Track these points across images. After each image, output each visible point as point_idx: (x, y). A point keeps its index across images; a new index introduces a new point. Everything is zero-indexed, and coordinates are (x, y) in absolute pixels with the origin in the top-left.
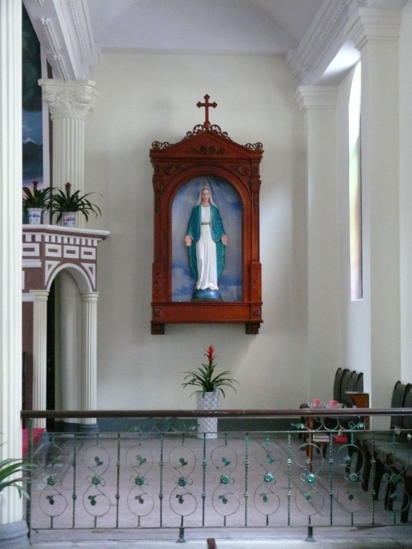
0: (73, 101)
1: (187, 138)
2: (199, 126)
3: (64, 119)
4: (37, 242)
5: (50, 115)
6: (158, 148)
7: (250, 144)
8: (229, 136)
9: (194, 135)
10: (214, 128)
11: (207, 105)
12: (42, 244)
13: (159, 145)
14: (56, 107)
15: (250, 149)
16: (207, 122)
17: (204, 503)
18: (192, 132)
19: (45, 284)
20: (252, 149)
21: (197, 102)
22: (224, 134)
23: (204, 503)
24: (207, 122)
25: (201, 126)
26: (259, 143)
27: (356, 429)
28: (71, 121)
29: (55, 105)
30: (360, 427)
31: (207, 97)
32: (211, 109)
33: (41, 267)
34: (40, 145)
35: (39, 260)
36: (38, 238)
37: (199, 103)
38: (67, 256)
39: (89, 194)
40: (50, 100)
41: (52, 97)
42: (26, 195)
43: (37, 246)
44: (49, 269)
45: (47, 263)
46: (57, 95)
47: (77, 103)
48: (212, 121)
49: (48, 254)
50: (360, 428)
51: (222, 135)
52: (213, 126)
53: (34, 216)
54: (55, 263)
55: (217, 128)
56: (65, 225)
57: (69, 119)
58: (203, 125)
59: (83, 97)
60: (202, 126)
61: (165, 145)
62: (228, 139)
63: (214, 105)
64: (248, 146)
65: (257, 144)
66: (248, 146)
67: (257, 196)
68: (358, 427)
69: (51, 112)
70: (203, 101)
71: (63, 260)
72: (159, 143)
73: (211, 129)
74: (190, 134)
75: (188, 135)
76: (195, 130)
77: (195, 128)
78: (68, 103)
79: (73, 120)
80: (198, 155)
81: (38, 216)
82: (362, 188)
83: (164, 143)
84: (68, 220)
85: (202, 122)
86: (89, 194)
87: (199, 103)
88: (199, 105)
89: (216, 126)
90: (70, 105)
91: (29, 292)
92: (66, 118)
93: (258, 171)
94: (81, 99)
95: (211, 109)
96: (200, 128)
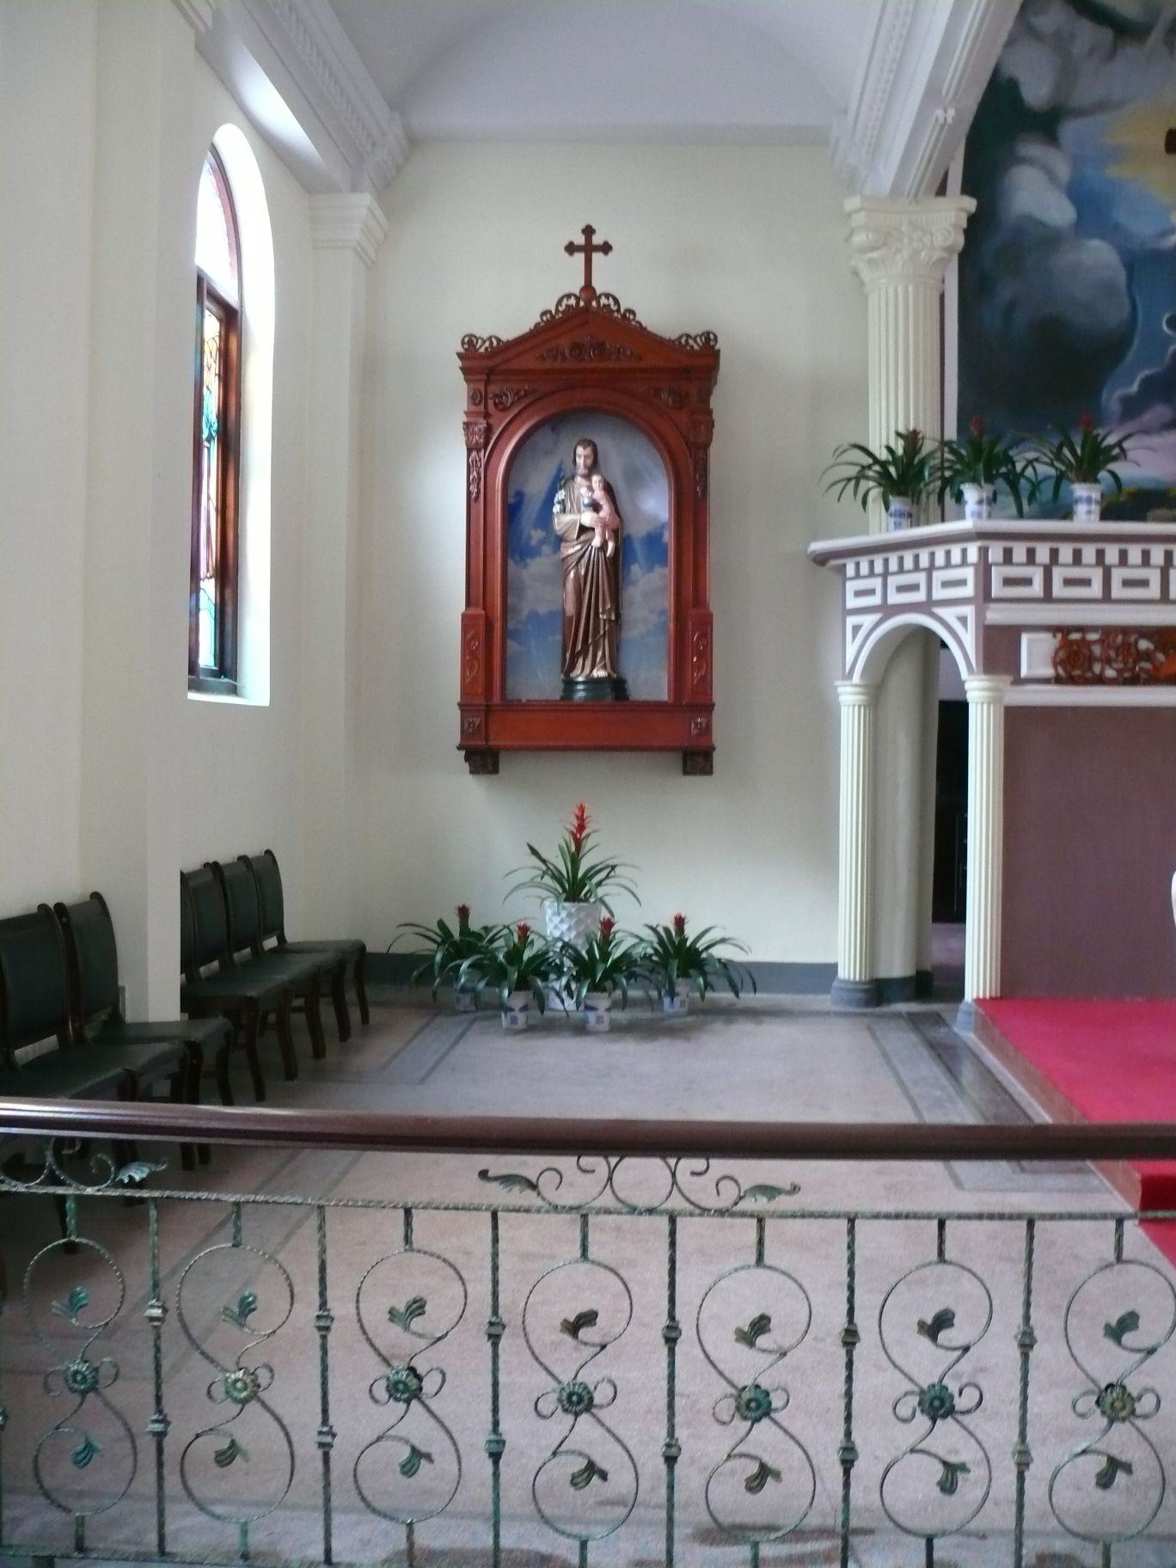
1: (542, 324)
2: (568, 296)
4: (1155, 567)
6: (477, 350)
7: (688, 336)
8: (638, 318)
9: (557, 317)
10: (603, 301)
11: (588, 249)
13: (477, 342)
15: (688, 348)
16: (588, 287)
17: (495, 1356)
18: (553, 312)
20: (692, 347)
21: (566, 243)
22: (627, 315)
23: (495, 1356)
24: (588, 287)
25: (573, 298)
26: (708, 333)
27: (122, 1185)
30: (131, 1178)
31: (589, 231)
32: (597, 257)
37: (571, 244)
38: (895, 598)
44: (854, 637)
48: (599, 286)
50: (133, 1184)
51: (624, 316)
52: (603, 298)
54: (868, 620)
55: (611, 301)
58: (577, 293)
60: (575, 296)
61: (491, 343)
62: (638, 325)
63: (606, 248)
64: (683, 341)
65: (703, 334)
66: (683, 341)
67: (704, 456)
68: (126, 1181)
70: (580, 240)
71: (887, 610)
72: (477, 339)
73: (598, 302)
74: (548, 316)
75: (545, 318)
76: (561, 306)
77: (559, 302)
80: (569, 365)
83: (490, 338)
85: (576, 285)
87: (571, 244)
88: (571, 249)
89: (607, 296)
93: (471, 393)
95: (597, 257)
96: (573, 301)
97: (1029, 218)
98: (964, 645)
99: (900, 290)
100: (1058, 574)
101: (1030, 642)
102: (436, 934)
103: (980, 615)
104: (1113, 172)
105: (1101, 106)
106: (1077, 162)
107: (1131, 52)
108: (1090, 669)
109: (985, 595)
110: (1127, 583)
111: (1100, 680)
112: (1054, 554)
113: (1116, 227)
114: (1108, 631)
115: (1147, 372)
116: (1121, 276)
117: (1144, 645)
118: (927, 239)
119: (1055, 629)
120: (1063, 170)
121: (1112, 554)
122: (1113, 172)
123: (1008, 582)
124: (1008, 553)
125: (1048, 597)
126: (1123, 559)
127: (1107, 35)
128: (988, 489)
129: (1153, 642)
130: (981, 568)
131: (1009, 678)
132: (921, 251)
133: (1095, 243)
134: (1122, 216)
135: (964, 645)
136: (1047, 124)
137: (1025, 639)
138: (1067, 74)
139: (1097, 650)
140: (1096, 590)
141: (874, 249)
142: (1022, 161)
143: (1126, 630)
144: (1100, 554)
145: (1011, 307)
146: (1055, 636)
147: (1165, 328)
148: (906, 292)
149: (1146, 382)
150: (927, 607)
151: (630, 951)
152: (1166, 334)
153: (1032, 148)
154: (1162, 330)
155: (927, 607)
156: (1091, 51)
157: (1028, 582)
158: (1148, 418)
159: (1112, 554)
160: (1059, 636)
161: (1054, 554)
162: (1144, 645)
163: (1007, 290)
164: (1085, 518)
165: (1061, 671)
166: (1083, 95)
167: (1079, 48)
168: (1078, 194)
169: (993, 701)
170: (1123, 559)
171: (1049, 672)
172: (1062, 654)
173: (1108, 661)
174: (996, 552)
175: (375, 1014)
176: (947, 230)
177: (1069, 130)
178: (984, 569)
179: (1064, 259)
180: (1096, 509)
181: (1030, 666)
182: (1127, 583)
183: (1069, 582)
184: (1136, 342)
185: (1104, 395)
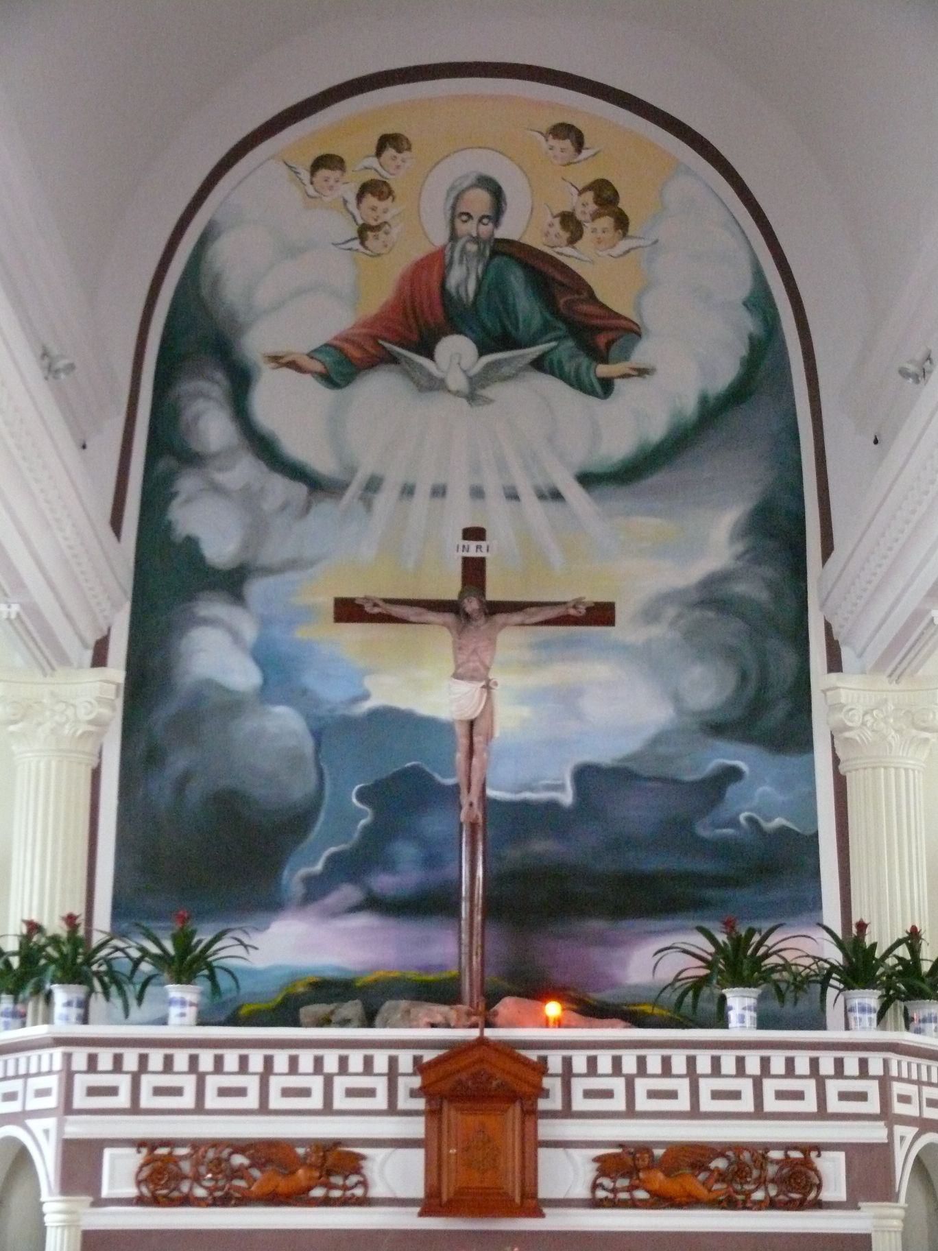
0: (904, 727)
3: (882, 770)
4: (874, 1078)
5: (836, 761)
12: (885, 1082)
14: (862, 740)
19: (897, 1190)
28: (897, 776)
29: (859, 736)
33: (886, 1141)
34: (813, 832)
35: (882, 1123)
36: (876, 1067)
39: (696, 968)
40: (849, 724)
41: (856, 718)
42: (847, 963)
43: (872, 1087)
45: (899, 1130)
46: (865, 713)
47: (914, 732)
49: (899, 1108)
53: (863, 1010)
54: (910, 1131)
56: (918, 1031)
57: (893, 771)
59: (931, 716)
69: (839, 754)
78: (893, 733)
79: (903, 772)
81: (870, 1010)
82: (793, 951)
84: (924, 1021)
86: (696, 968)
90: (898, 737)
91: (859, 1209)
92: (885, 768)
94: (924, 721)
97: (209, 683)
98: (47, 1163)
99: (42, 765)
100: (147, 1082)
101: (113, 1158)
103: (61, 1126)
104: (302, 633)
105: (292, 565)
106: (265, 622)
107: (325, 508)
108: (177, 1188)
109: (68, 1108)
110: (223, 1092)
111: (187, 1201)
112: (143, 1059)
113: (305, 692)
115: (333, 849)
116: (309, 745)
117: (239, 1160)
118: (70, 712)
119: (140, 1144)
120: (249, 632)
121: (206, 1060)
122: (302, 633)
123: (93, 1091)
124: (92, 1060)
125: (135, 1109)
126: (839, 1072)
127: (299, 490)
128: (78, 991)
129: (248, 1157)
130: (64, 1074)
131: (90, 1199)
132: (65, 724)
133: (281, 710)
134: (310, 680)
137: (108, 1153)
138: (257, 530)
139: (186, 1167)
140: (188, 1101)
141: (14, 722)
142: (206, 622)
143: (216, 1144)
144: (194, 1060)
145: (183, 781)
146: (139, 1152)
147: (354, 800)
148: (48, 768)
149: (333, 859)
152: (356, 807)
153: (214, 607)
154: (350, 802)
156: (284, 507)
157: (112, 1091)
159: (331, 1061)
160: (144, 1151)
161: (143, 1059)
162: (239, 1160)
163: (179, 761)
164: (181, 1023)
165: (145, 1190)
166: (274, 551)
167: (270, 504)
168: (264, 656)
169: (68, 1225)
170: (839, 1072)
171: (131, 1191)
172: (146, 1172)
173: (197, 1179)
174: (80, 1058)
176: (90, 703)
177: (256, 589)
178: (69, 1076)
179: (247, 725)
180: (191, 1012)
181: (112, 1186)
182: (223, 1092)
183: (159, 1091)
184: (322, 816)
185: (286, 873)
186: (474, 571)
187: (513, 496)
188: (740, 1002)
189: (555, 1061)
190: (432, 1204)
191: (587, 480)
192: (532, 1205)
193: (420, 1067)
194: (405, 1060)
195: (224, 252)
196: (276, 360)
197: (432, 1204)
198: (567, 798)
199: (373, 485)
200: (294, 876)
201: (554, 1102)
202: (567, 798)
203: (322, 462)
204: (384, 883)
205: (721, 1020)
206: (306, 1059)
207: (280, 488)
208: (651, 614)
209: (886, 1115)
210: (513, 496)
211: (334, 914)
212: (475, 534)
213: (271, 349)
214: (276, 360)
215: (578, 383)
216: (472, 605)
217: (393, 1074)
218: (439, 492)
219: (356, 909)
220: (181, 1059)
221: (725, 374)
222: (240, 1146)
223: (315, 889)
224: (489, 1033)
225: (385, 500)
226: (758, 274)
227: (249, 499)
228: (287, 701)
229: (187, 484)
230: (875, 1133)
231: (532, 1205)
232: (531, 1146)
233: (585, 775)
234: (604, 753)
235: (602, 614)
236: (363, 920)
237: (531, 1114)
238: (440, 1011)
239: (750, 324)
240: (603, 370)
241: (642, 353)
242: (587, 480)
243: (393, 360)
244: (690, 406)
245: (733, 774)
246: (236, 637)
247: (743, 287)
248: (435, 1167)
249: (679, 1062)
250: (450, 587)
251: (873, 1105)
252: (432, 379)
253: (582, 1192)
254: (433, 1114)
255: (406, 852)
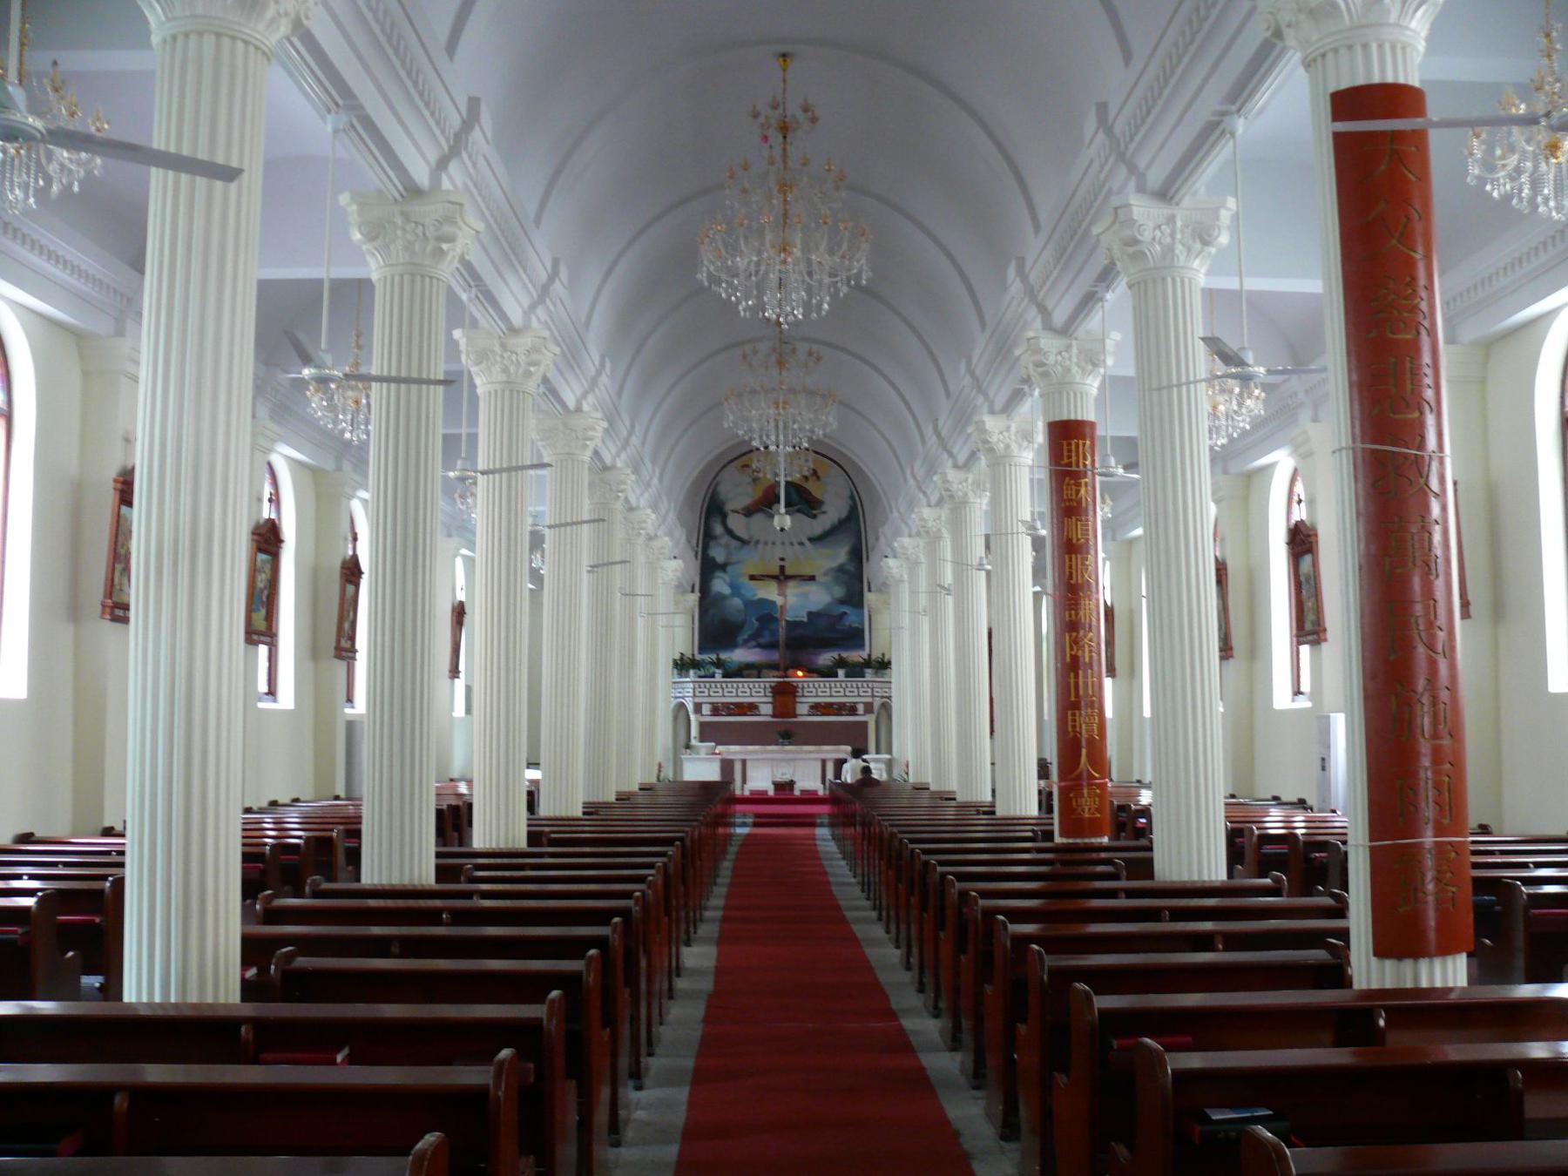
12: (872, 689)
98: (690, 707)
102: (1357, 11)
105: (738, 562)
109: (694, 696)
114: (723, 703)
120: (728, 580)
125: (709, 696)
127: (739, 543)
134: (743, 591)
135: (690, 707)
136: (723, 567)
142: (718, 577)
143: (727, 703)
150: (683, 698)
151: (1293, 522)
153: (719, 574)
155: (683, 698)
158: (750, 644)
163: (712, 611)
164: (718, 677)
166: (734, 559)
168: (732, 586)
175: (357, 796)
177: (729, 569)
178: (694, 689)
179: (728, 603)
186: (782, 568)
187: (792, 544)
188: (841, 672)
189: (800, 685)
190: (774, 716)
191: (811, 540)
192: (795, 716)
193: (771, 687)
194: (768, 685)
195: (719, 488)
196: (733, 511)
197: (774, 716)
198: (805, 620)
199: (757, 542)
200: (740, 639)
201: (800, 694)
202: (805, 620)
203: (745, 536)
204: (762, 641)
205: (836, 676)
206: (746, 685)
207: (734, 543)
208: (825, 574)
209: (873, 696)
210: (792, 544)
211: (750, 648)
212: (782, 559)
213: (733, 508)
214: (733, 511)
215: (808, 516)
216: (782, 578)
217: (765, 687)
218: (774, 543)
219: (755, 647)
220: (719, 685)
221: (844, 514)
222: (732, 704)
223: (745, 643)
224: (786, 679)
225: (760, 546)
226: (852, 493)
227: (727, 546)
228: (738, 596)
229: (712, 544)
230: (870, 700)
231: (795, 716)
232: (795, 703)
233: (810, 614)
234: (814, 609)
235: (812, 578)
236: (757, 650)
237: (795, 696)
238: (776, 673)
239: (850, 502)
240: (814, 512)
241: (824, 508)
242: (811, 540)
243: (762, 510)
244: (836, 520)
245: (845, 613)
246: (724, 581)
247: (848, 494)
248: (774, 708)
249: (827, 685)
250: (776, 571)
251: (870, 694)
252: (785, 185)
253: (806, 713)
254: (774, 697)
255: (766, 633)
